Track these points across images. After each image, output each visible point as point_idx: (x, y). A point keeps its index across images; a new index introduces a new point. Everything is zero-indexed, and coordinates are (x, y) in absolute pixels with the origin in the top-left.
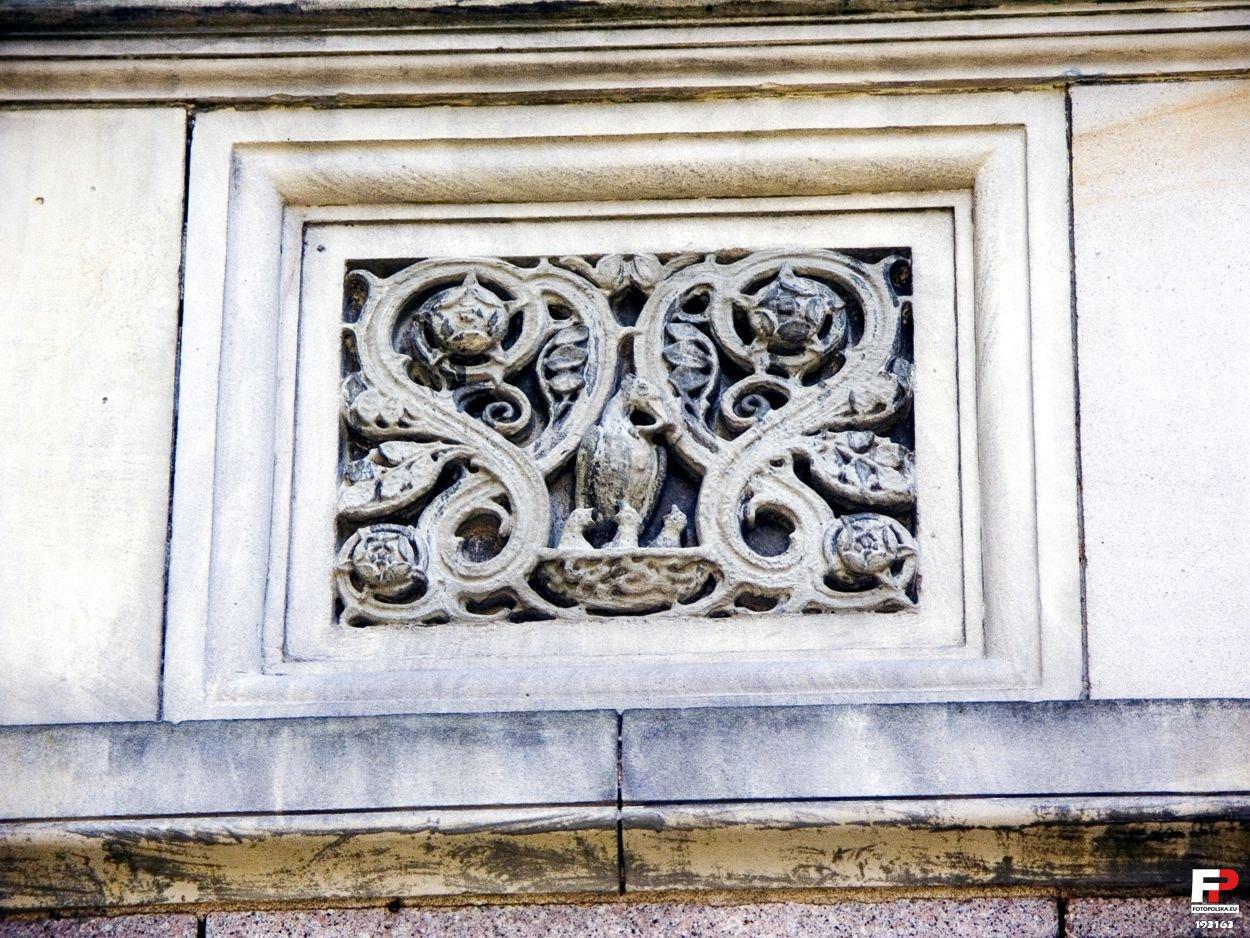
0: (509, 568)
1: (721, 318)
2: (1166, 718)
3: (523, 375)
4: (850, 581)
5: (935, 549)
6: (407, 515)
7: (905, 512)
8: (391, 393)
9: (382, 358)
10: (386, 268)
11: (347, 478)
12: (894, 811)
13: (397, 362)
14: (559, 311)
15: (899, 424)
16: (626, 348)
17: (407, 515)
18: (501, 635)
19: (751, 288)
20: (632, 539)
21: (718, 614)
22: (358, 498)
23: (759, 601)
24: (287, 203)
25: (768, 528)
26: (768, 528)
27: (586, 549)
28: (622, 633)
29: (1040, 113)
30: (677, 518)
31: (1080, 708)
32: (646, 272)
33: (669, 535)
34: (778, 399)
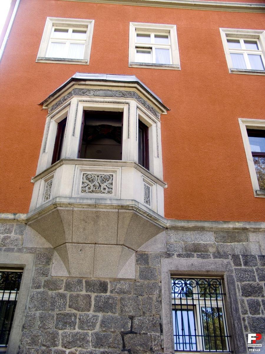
0: (91, 190)
3: (92, 180)
4: (109, 192)
5: (113, 191)
6: (85, 187)
7: (112, 189)
8: (85, 180)
9: (85, 178)
10: (85, 174)
11: (82, 185)
15: (112, 184)
16: (98, 179)
17: (85, 187)
18: (90, 194)
20: (97, 189)
21: (101, 193)
22: (83, 186)
23: (104, 193)
25: (104, 189)
27: (95, 189)
28: (96, 194)
31: (120, 200)
32: (99, 175)
34: (105, 182)
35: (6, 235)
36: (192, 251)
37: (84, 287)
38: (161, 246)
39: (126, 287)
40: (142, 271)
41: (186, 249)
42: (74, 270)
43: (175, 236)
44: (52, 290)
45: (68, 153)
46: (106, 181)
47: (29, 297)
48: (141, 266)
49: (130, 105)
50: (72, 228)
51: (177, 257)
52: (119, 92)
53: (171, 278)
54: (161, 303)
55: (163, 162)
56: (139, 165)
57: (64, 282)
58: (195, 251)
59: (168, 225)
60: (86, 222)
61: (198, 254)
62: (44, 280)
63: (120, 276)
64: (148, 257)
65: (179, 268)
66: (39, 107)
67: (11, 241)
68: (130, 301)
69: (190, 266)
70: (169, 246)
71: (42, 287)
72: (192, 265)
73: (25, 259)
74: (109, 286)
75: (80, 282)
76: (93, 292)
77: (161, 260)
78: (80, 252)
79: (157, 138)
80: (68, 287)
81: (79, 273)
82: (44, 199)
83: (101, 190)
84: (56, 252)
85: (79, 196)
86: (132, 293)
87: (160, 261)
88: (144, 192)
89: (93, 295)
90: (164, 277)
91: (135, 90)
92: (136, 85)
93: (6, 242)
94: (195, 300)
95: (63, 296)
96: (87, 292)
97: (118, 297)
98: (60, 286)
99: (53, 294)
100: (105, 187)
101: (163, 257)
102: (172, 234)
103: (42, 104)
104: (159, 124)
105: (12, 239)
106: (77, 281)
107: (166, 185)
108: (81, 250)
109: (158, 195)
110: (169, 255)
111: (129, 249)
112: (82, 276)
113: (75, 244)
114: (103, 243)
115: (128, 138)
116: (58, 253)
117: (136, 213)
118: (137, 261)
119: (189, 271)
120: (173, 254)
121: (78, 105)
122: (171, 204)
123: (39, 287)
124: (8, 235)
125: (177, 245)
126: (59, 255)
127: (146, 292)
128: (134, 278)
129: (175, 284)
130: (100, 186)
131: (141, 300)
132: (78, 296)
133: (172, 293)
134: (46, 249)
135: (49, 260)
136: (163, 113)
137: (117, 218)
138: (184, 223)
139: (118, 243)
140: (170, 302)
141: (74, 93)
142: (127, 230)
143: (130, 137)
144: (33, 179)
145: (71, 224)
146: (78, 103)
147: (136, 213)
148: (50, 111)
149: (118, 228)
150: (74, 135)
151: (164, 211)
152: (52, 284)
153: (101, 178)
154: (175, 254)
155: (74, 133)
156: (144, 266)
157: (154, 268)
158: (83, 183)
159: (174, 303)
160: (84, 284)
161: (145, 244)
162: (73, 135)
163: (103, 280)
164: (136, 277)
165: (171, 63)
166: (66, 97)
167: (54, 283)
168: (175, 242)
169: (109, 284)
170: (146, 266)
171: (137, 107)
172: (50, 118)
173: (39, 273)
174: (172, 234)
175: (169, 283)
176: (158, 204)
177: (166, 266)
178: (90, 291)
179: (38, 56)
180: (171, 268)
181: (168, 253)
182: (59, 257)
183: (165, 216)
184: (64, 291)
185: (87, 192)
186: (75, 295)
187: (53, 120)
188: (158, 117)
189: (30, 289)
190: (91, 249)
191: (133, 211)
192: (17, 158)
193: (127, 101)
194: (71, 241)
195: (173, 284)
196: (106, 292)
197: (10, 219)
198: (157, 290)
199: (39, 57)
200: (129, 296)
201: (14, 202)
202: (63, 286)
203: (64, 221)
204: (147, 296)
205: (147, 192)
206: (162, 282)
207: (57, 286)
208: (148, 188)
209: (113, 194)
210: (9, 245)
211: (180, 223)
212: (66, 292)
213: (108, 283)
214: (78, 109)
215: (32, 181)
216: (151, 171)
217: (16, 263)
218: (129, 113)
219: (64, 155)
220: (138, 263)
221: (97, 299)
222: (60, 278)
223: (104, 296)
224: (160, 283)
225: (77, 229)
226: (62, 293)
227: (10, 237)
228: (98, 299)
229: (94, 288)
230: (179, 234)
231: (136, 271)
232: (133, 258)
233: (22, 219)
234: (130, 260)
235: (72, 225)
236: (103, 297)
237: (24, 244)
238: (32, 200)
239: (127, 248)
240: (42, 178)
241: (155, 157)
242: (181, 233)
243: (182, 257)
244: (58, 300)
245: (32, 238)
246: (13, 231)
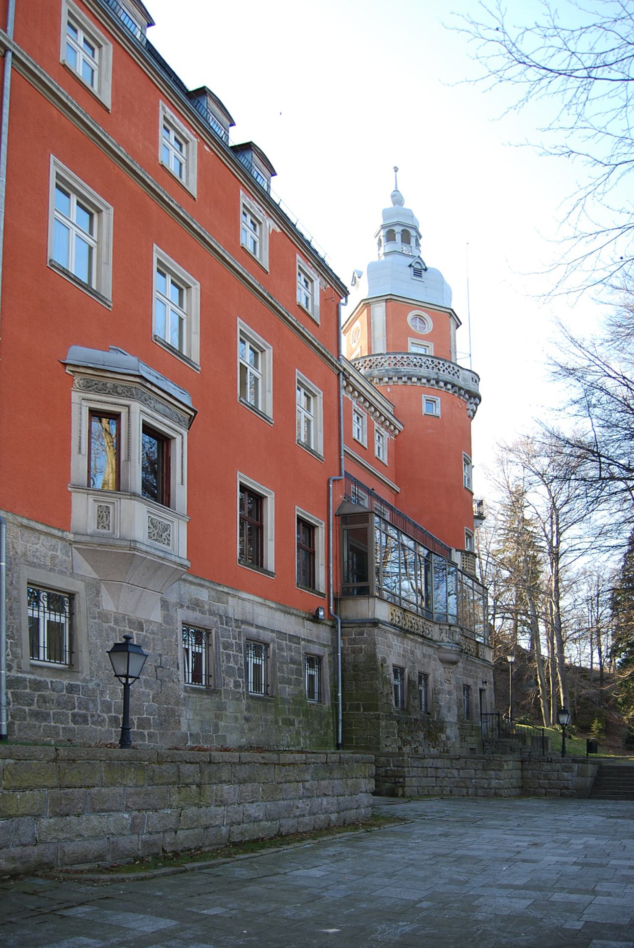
80: (116, 622)
97: (151, 636)
123: (95, 618)
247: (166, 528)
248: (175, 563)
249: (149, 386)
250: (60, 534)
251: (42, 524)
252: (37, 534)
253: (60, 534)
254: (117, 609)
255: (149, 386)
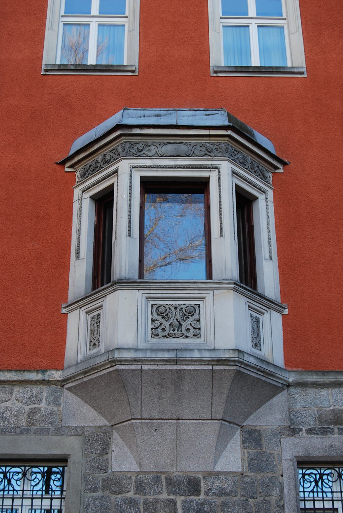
0: (166, 333)
1: (183, 310)
2: (222, 351)
3: (167, 315)
4: (195, 335)
5: (202, 332)
6: (157, 328)
7: (199, 329)
8: (156, 317)
9: (155, 313)
10: (155, 304)
11: (152, 324)
12: (199, 359)
13: (156, 314)
14: (170, 309)
15: (199, 320)
16: (176, 313)
17: (157, 328)
18: (166, 340)
19: (186, 307)
20: (177, 330)
21: (184, 338)
22: (153, 327)
23: (187, 337)
24: (147, 298)
25: (188, 330)
26: (188, 330)
27: (172, 332)
28: (176, 340)
29: (211, 292)
30: (180, 329)
31: (214, 349)
32: (177, 306)
33: (180, 331)
34: (189, 318)
35: (33, 406)
36: (331, 423)
37: (164, 487)
38: (281, 416)
39: (228, 485)
40: (252, 459)
41: (320, 419)
42: (147, 462)
43: (303, 399)
44: (115, 493)
45: (123, 269)
46: (190, 317)
47: (82, 505)
48: (250, 451)
49: (221, 172)
50: (140, 395)
51: (307, 434)
52: (201, 147)
53: (298, 468)
54: (284, 509)
55: (279, 267)
56: (241, 285)
57: (133, 480)
58: (336, 423)
59: (290, 380)
60: (162, 387)
61: (341, 429)
62: (101, 478)
63: (218, 468)
64: (260, 435)
65: (311, 452)
66: (58, 168)
67: (43, 416)
68: (236, 507)
69: (327, 448)
70: (294, 415)
71: (101, 490)
72: (331, 446)
73: (70, 445)
74: (202, 485)
75: (157, 479)
76: (179, 494)
77: (282, 440)
78: (155, 434)
79: (268, 223)
80: (140, 487)
81: (155, 465)
82: (88, 346)
83: (183, 332)
84: (116, 433)
85: (148, 346)
86: (239, 495)
87: (280, 441)
88: (251, 329)
89: (179, 500)
90: (287, 467)
91: (227, 140)
92: (229, 132)
93: (35, 418)
94: (336, 500)
95: (132, 503)
96: (169, 495)
97: (218, 501)
98: (127, 488)
99: (118, 499)
100: (189, 327)
101: (284, 435)
102: (297, 393)
103: (63, 163)
104: (270, 193)
105: (44, 413)
106: (153, 479)
107: (285, 309)
108: (156, 430)
109: (273, 324)
110: (293, 431)
111: (231, 425)
112: (160, 471)
113: (147, 421)
114: (190, 418)
115: (221, 236)
116: (119, 435)
117: (241, 369)
118: (244, 443)
119: (326, 456)
120: (301, 430)
121: (131, 175)
122: (295, 342)
123: (95, 490)
124: (36, 406)
125: (306, 413)
126: (122, 438)
127: (260, 493)
128: (240, 470)
129: (304, 475)
130: (181, 325)
131: (252, 505)
132: (156, 501)
133: (300, 492)
134: (100, 427)
135: (106, 447)
136: (277, 171)
137: (211, 380)
138: (318, 376)
139: (213, 418)
140: (298, 506)
141: (122, 152)
142: (228, 397)
143: (223, 234)
144: (64, 308)
145: (140, 390)
146: (131, 172)
147: (241, 369)
148: (80, 179)
149: (212, 394)
150: (130, 234)
151: (284, 356)
152: (115, 484)
153: (181, 312)
154: (304, 429)
155: (129, 230)
156: (255, 450)
157: (270, 453)
158: (153, 321)
159: (304, 507)
160: (164, 483)
161: (254, 414)
162: (129, 235)
163: (192, 476)
164: (243, 468)
165: (289, 65)
166: (108, 158)
167: (117, 483)
168: (303, 409)
169: (202, 480)
170: (259, 451)
171: (234, 172)
172: (81, 192)
173: (93, 467)
174: (298, 395)
175: (295, 477)
176: (274, 347)
177: (289, 450)
178: (174, 494)
179: (44, 63)
180: (298, 452)
181: (292, 427)
182: (120, 441)
183: (286, 364)
184: (135, 494)
185: (160, 336)
186: (151, 500)
187: (87, 195)
188: (268, 180)
189: (83, 493)
190: (171, 428)
191: (236, 367)
192: (33, 269)
193: (215, 163)
194: (140, 417)
195: (301, 476)
196: (199, 495)
197: (37, 381)
198: (278, 489)
199: (46, 65)
200: (235, 498)
201: (38, 349)
202: (132, 487)
203: (127, 386)
204: (262, 498)
205: (255, 327)
206: (284, 475)
207: (123, 487)
208: (257, 320)
209: (202, 339)
210: (39, 424)
211: (311, 377)
212: (137, 496)
213: (200, 480)
214: (132, 182)
215: (64, 311)
216: (259, 290)
217: (58, 453)
218: (220, 187)
219: (118, 272)
220: (245, 445)
221: (185, 506)
222: (126, 475)
223: (195, 500)
224: (281, 478)
225: (149, 398)
226: (130, 498)
227: (39, 410)
228: (187, 505)
229: (179, 488)
230: (309, 395)
231: (243, 460)
232: (237, 438)
233: (55, 379)
234: (232, 441)
235: (140, 392)
236: (195, 502)
237: (64, 421)
238: (68, 345)
239: (227, 423)
240: (80, 308)
241: (265, 259)
242: (311, 391)
243: (315, 434)
244: (127, 509)
245: (76, 411)
246: (44, 400)
247: (192, 312)
248: (202, 361)
249: (138, 131)
250: (40, 376)
251: (10, 370)
252: (8, 388)
253: (40, 376)
254: (140, 465)
255: (138, 131)
